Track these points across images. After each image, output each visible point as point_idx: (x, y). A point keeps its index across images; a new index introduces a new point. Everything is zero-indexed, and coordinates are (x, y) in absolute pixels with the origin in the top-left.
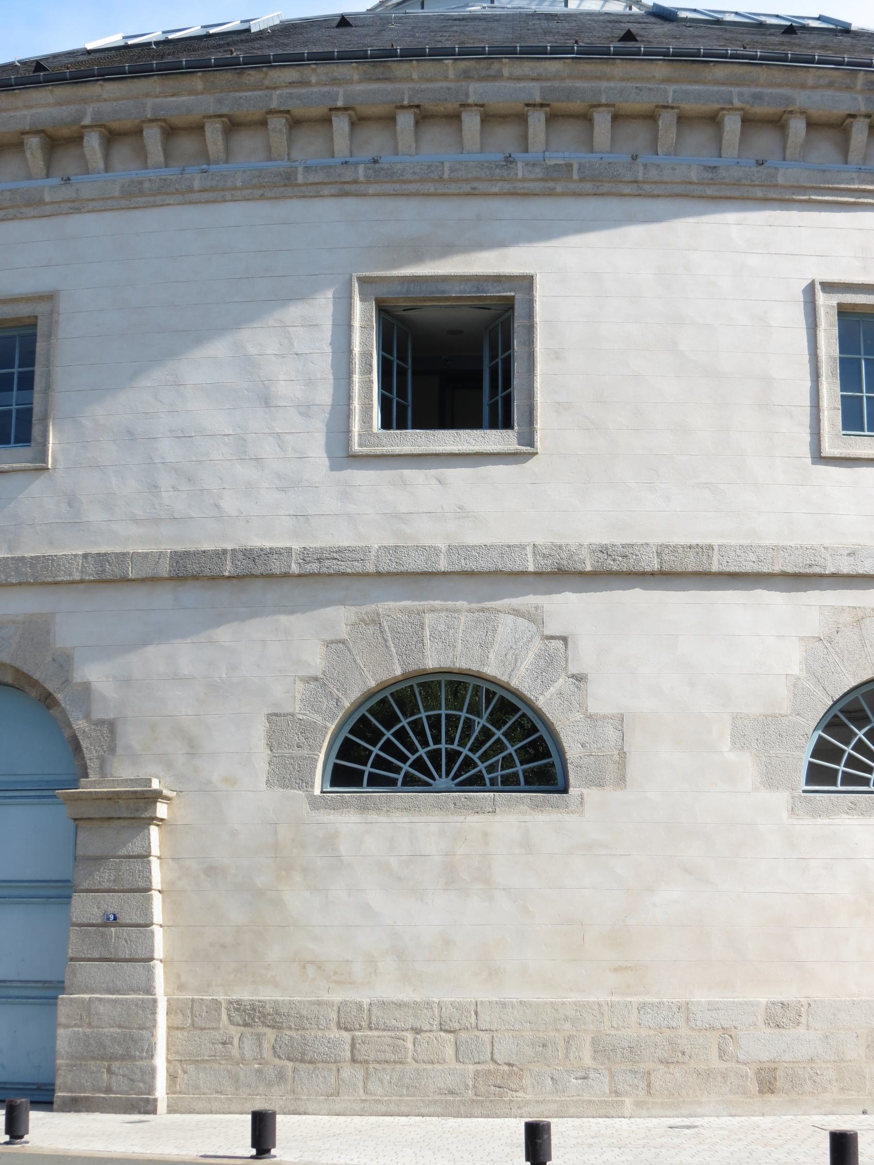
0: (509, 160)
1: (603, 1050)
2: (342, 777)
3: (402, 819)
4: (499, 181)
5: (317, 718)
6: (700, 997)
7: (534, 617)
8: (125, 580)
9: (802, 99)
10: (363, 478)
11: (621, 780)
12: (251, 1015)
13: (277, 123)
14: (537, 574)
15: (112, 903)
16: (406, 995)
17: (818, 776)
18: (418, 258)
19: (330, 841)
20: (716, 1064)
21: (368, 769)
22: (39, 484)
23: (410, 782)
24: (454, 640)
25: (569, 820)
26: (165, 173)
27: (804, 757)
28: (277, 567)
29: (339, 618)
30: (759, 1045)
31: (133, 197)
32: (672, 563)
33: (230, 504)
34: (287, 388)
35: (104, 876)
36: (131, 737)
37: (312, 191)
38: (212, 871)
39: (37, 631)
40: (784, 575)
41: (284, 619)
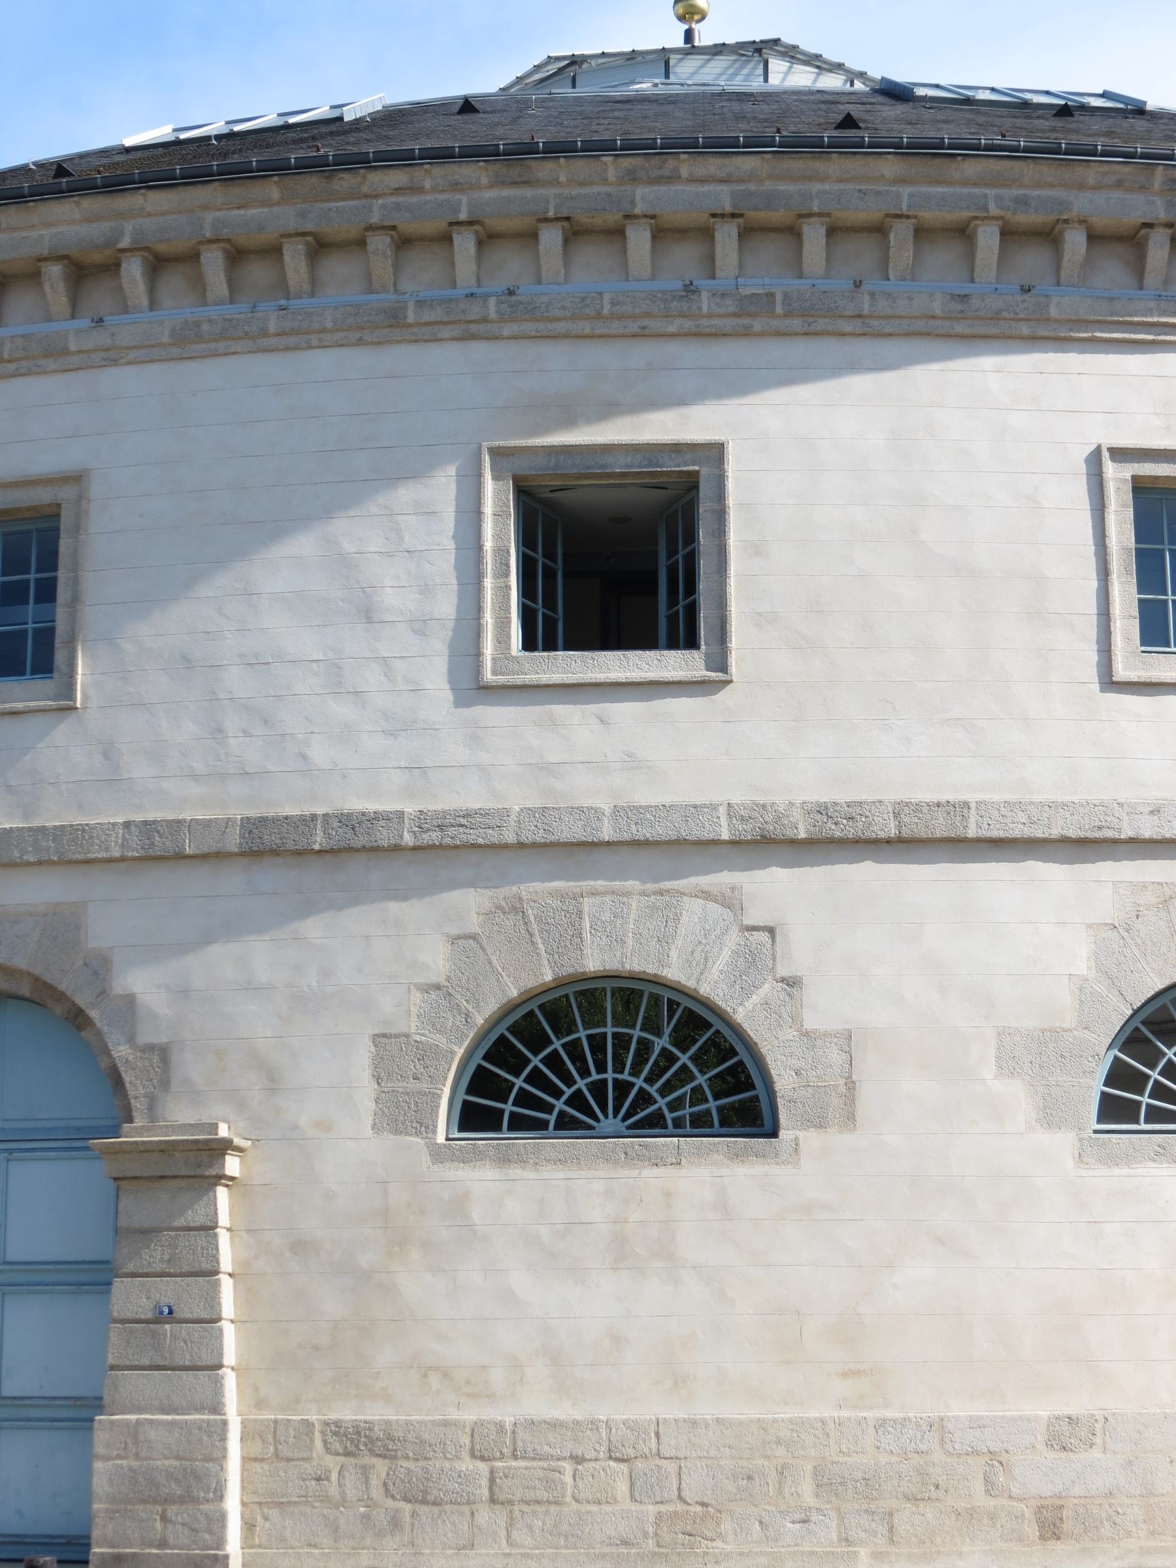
0: (690, 290)
1: (828, 1483)
2: (473, 1118)
3: (555, 1174)
4: (679, 317)
5: (441, 1040)
6: (959, 1410)
7: (730, 902)
8: (180, 857)
9: (1082, 203)
10: (498, 716)
11: (850, 1119)
12: (355, 1441)
13: (379, 243)
14: (733, 843)
15: (166, 1291)
16: (563, 1411)
17: (1114, 1110)
18: (569, 421)
19: (458, 1205)
20: (981, 1500)
21: (508, 1108)
22: (64, 729)
23: (566, 1124)
24: (679, 940)
25: (780, 1173)
26: (237, 311)
27: (1095, 1086)
28: (384, 837)
29: (469, 905)
30: (1039, 1475)
31: (188, 343)
32: (915, 827)
33: (321, 753)
34: (395, 597)
35: (155, 1255)
36: (191, 1066)
37: (427, 333)
38: (300, 1247)
39: (63, 926)
40: (1065, 841)
41: (394, 907)
